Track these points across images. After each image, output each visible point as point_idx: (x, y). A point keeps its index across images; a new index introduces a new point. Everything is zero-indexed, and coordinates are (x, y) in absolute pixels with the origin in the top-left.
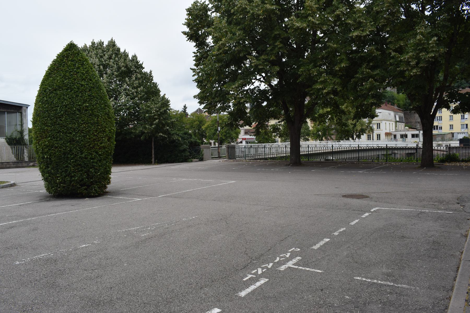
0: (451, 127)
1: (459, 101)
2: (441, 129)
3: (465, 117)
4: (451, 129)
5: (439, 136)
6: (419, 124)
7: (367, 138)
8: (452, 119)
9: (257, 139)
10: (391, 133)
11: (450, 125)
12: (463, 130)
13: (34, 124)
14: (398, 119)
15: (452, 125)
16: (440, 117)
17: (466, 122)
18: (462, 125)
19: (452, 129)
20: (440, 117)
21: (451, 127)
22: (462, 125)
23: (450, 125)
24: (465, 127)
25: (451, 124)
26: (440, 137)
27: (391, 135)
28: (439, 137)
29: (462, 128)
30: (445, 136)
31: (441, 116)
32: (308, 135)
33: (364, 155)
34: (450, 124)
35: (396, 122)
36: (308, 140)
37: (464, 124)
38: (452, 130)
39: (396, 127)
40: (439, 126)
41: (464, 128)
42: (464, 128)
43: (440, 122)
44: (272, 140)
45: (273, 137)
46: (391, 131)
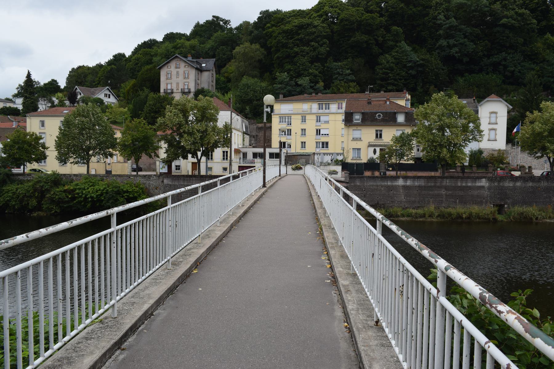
0: (303, 144)
1: (220, 23)
2: (290, 147)
3: (321, 133)
4: (302, 147)
5: (302, 157)
6: (253, 139)
7: (222, 157)
8: (305, 135)
9: (6, 150)
10: (239, 150)
11: (302, 143)
12: (318, 150)
13: (20, 159)
14: (244, 130)
15: (305, 143)
16: (288, 130)
17: (324, 139)
18: (317, 142)
19: (305, 147)
20: (288, 130)
21: (303, 144)
22: (317, 142)
23: (302, 143)
24: (321, 146)
25: (303, 141)
26: (305, 159)
27: (239, 153)
28: (301, 158)
29: (317, 147)
30: (310, 157)
31: (290, 130)
32: (113, 146)
33: (285, 168)
34: (302, 141)
35: (244, 133)
36: (111, 155)
37: (319, 142)
38: (303, 149)
39: (244, 140)
40: (286, 143)
41: (319, 147)
42: (319, 147)
43: (289, 137)
44: (38, 152)
45: (40, 148)
46: (239, 147)
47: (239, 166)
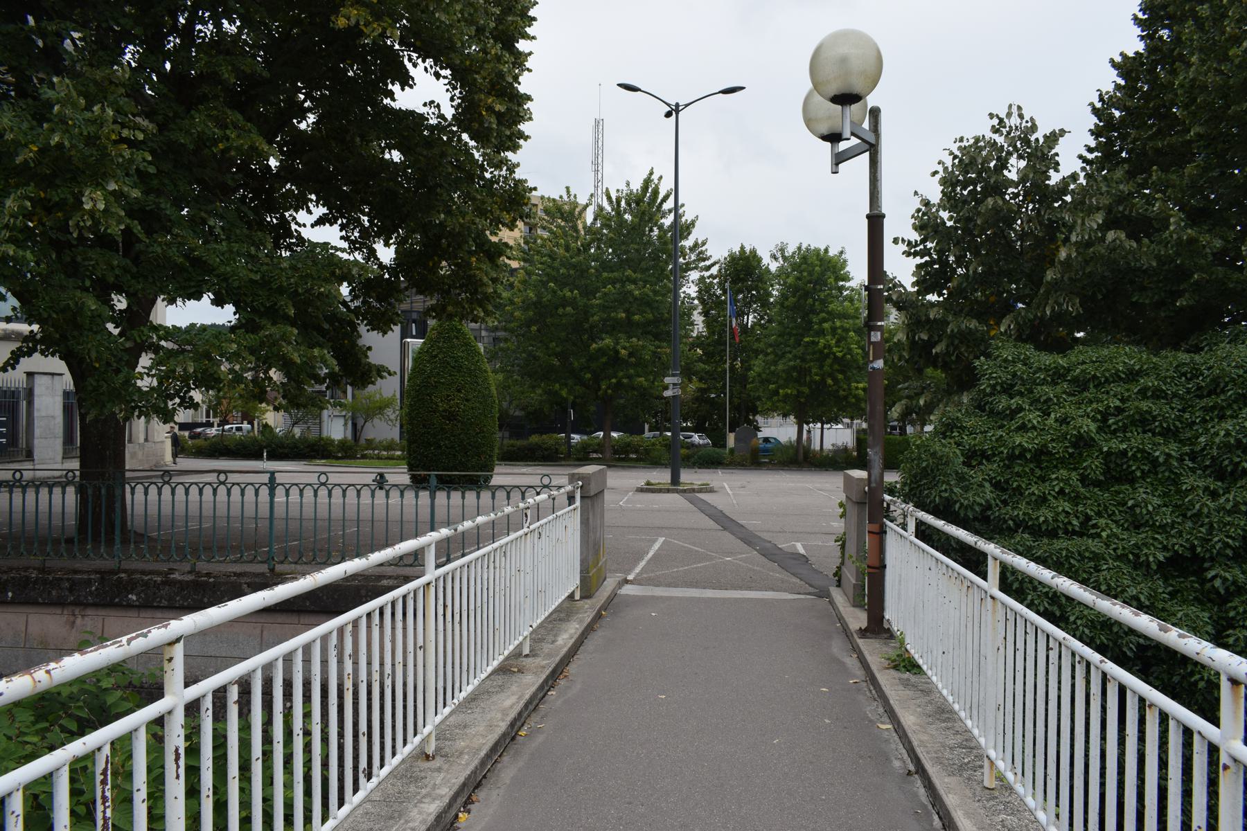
47: (29, 455)
